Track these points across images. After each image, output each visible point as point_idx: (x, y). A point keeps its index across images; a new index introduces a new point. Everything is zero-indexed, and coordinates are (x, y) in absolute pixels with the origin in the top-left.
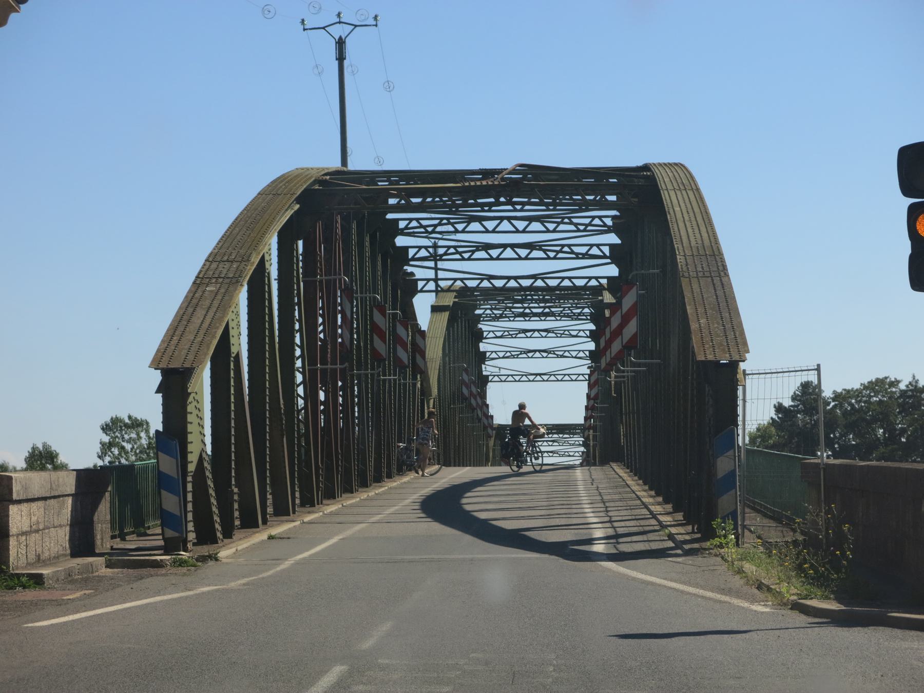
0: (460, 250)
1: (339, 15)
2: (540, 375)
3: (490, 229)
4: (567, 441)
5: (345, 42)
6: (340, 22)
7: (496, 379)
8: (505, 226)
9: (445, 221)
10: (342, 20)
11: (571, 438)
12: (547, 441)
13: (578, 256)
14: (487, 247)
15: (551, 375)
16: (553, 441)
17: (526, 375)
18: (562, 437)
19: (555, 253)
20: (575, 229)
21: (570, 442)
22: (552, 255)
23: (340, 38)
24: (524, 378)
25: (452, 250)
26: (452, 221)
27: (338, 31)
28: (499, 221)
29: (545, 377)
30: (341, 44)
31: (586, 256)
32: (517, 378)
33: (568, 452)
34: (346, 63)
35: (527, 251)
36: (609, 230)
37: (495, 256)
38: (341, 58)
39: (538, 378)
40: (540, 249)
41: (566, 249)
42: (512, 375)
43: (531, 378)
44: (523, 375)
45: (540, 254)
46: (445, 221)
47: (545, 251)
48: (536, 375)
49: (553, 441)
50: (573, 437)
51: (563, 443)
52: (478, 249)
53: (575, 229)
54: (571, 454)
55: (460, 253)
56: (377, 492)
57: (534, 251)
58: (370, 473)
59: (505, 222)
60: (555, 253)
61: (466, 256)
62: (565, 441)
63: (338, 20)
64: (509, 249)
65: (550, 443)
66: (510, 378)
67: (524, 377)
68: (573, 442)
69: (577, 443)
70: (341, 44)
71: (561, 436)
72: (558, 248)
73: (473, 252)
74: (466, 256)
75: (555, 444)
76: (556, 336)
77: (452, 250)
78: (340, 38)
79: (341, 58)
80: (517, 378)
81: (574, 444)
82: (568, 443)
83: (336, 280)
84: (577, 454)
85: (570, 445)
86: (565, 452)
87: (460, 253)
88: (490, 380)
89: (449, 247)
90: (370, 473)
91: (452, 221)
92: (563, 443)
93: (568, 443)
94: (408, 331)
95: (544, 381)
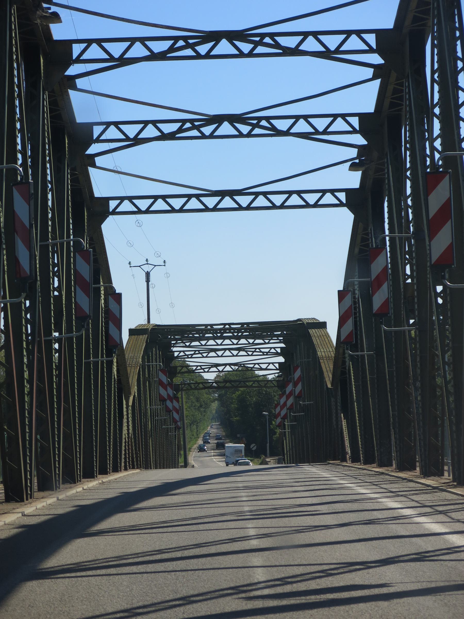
0: (203, 367)
1: (147, 260)
2: (232, 193)
3: (220, 355)
4: (259, 349)
5: (150, 273)
6: (147, 264)
7: (126, 206)
8: (227, 353)
9: (197, 352)
10: (148, 263)
11: (265, 343)
12: (230, 349)
13: (264, 354)
14: (215, 350)
15: (257, 194)
16: (239, 349)
17: (198, 196)
18: (253, 343)
19: (252, 353)
20: (261, 349)
21: (262, 350)
22: (250, 353)
23: (147, 272)
24: (194, 204)
25: (199, 368)
26: (201, 352)
27: (147, 268)
28: (224, 351)
29: (244, 200)
30: (148, 275)
31: (267, 353)
32: (177, 203)
33: (258, 364)
34: (150, 283)
35: (236, 352)
36: (277, 354)
37: (220, 355)
38: (148, 281)
39: (227, 202)
40: (244, 351)
41: (258, 350)
42: (164, 197)
43: (211, 202)
44: (189, 197)
45: (244, 353)
46: (197, 352)
47: (246, 352)
48: (222, 194)
49: (239, 349)
50: (268, 343)
51: (253, 352)
52: (212, 366)
53: (261, 349)
54: (264, 366)
55: (203, 369)
56: (104, 480)
57: (241, 352)
58: (79, 469)
59: (227, 351)
60: (252, 353)
61: (206, 370)
62: (256, 349)
63: (146, 263)
64: (228, 366)
65: (235, 353)
66: (160, 205)
67: (194, 200)
68: (267, 350)
69: (273, 351)
70: (148, 275)
71: (251, 341)
72: (254, 350)
73: (210, 368)
74: (206, 370)
75: (242, 353)
76: (278, 39)
77: (199, 368)
78: (147, 272)
79: (148, 281)
80: (177, 203)
81: (269, 352)
82: (261, 352)
83: (72, 338)
84: (271, 367)
85: (264, 355)
86: (255, 364)
87: (203, 369)
88: (111, 208)
89: (197, 366)
90: (79, 469)
91: (201, 352)
92: (253, 352)
93: (261, 352)
94: (76, 303)
95: (240, 208)
